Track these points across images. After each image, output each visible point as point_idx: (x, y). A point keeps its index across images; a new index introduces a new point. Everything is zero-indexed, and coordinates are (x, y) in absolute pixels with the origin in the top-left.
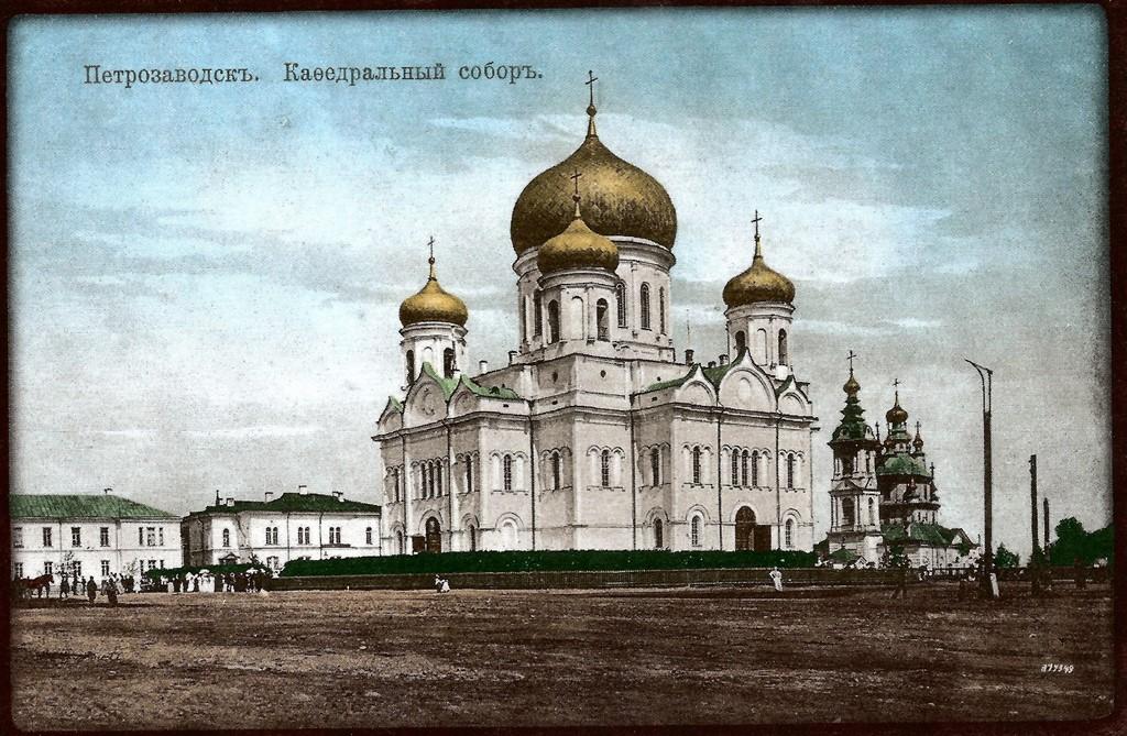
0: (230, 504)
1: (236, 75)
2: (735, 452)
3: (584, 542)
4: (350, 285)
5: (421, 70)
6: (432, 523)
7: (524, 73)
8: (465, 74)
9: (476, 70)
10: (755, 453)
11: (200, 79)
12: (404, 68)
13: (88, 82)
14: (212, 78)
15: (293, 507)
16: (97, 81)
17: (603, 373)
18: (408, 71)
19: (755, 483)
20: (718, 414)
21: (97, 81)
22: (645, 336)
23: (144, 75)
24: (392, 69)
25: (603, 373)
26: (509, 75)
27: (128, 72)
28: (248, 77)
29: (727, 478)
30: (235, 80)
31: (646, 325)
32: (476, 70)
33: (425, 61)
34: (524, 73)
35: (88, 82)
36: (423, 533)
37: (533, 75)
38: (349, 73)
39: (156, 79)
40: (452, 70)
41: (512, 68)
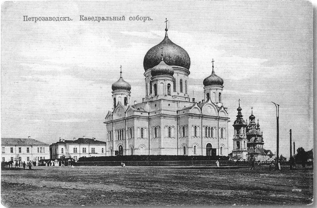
0: (64, 141)
1: (66, 19)
2: (206, 127)
6: (121, 147)
7: (148, 19)
8: (131, 19)
9: (138, 19)
10: (212, 128)
12: (114, 17)
14: (59, 19)
17: (169, 105)
19: (212, 136)
20: (202, 116)
22: (181, 94)
25: (169, 105)
26: (143, 19)
29: (204, 135)
31: (181, 91)
32: (138, 19)
33: (119, 16)
38: (98, 18)
40: (127, 18)
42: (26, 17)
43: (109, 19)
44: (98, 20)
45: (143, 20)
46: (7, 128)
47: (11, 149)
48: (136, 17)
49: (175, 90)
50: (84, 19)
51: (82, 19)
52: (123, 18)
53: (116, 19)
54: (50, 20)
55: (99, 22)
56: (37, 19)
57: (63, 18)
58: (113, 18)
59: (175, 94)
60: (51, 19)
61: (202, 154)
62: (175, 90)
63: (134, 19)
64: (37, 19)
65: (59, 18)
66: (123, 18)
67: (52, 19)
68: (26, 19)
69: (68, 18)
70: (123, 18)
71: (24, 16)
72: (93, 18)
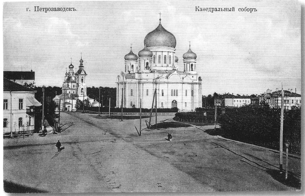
1: (71, 9)
3: (301, 72)
4: (253, 159)
5: (229, 9)
7: (254, 10)
8: (240, 10)
9: (242, 9)
11: (63, 10)
12: (225, 8)
13: (35, 11)
14: (66, 10)
15: (21, 86)
16: (38, 11)
18: (226, 9)
21: (251, 9)
23: (242, 10)
24: (222, 8)
26: (250, 10)
27: (217, 11)
28: (74, 10)
30: (71, 10)
31: (165, 63)
32: (242, 9)
33: (230, 7)
34: (254, 10)
35: (35, 11)
36: (212, 96)
37: (256, 10)
38: (211, 9)
39: (52, 10)
40: (236, 9)
41: (251, 9)
42: (37, 8)
43: (221, 10)
44: (211, 10)
45: (250, 11)
46: (138, 155)
47: (20, 101)
48: (244, 8)
49: (159, 62)
50: (199, 9)
51: (197, 9)
52: (233, 9)
53: (227, 10)
54: (58, 11)
55: (212, 12)
56: (47, 9)
57: (69, 9)
58: (224, 9)
59: (160, 65)
60: (220, 10)
61: (141, 106)
62: (159, 62)
63: (242, 10)
64: (47, 9)
65: (66, 9)
66: (233, 9)
67: (60, 9)
68: (37, 10)
69: (74, 9)
70: (233, 9)
71: (35, 7)
72: (41, 9)
